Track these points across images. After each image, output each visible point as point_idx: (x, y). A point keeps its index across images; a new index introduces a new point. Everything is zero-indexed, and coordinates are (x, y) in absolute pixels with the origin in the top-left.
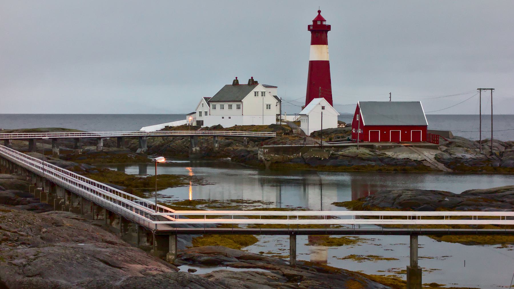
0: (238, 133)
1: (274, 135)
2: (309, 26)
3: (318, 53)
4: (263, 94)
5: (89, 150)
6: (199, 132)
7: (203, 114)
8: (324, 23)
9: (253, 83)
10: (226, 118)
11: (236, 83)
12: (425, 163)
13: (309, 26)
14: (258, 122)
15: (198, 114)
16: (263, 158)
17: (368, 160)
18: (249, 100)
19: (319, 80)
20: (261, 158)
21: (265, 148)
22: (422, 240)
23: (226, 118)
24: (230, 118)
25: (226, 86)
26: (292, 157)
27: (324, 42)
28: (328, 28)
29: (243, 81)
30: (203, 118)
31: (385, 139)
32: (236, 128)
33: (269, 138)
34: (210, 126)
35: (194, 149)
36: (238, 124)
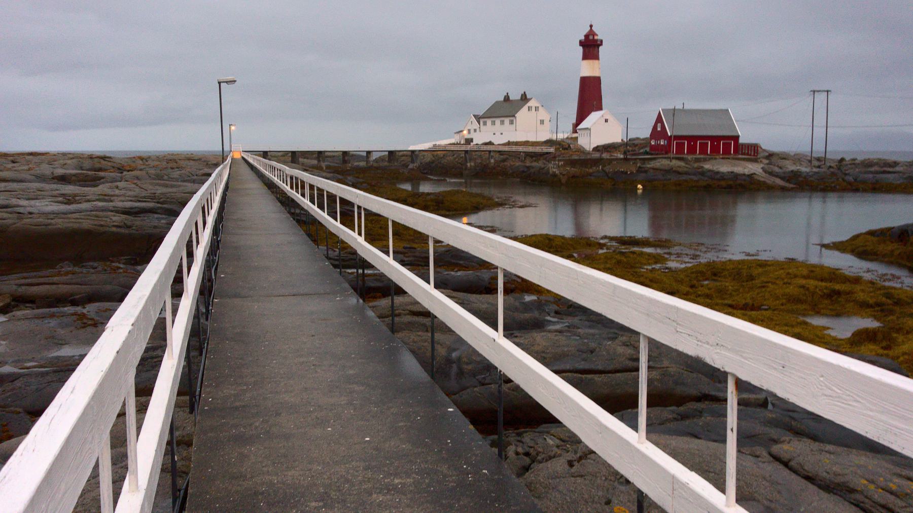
0: (514, 148)
1: (552, 150)
3: (588, 69)
4: (537, 109)
5: (358, 166)
6: (468, 148)
7: (472, 131)
8: (596, 38)
9: (524, 99)
10: (498, 134)
11: (507, 98)
12: (756, 177)
14: (532, 138)
15: (465, 132)
16: (557, 172)
17: (686, 173)
18: (523, 115)
19: (590, 96)
20: (554, 172)
21: (559, 161)
23: (498, 134)
25: (497, 102)
26: (591, 171)
27: (596, 57)
28: (601, 43)
29: (515, 96)
30: (473, 135)
31: (692, 150)
32: (509, 143)
33: (547, 153)
34: (480, 143)
35: (469, 165)
36: (511, 140)
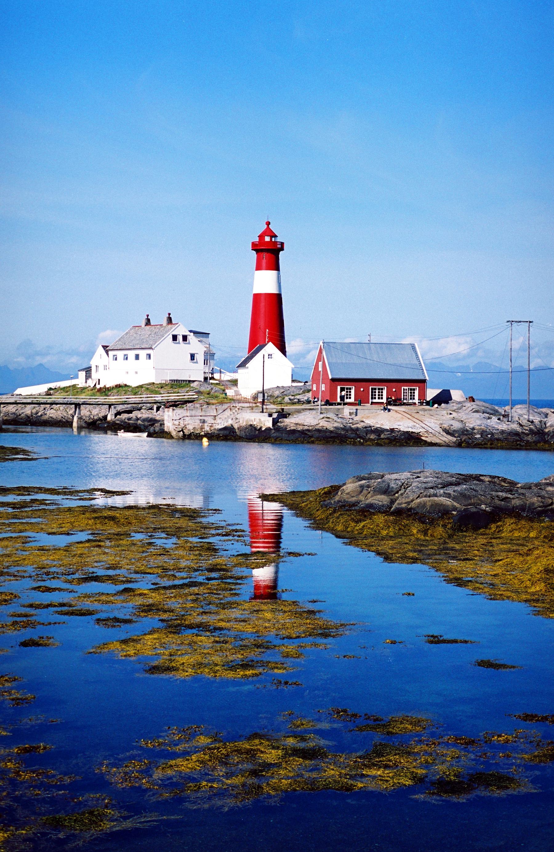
2: (253, 244)
3: (265, 282)
13: (253, 244)
19: (269, 321)
22: (262, 394)
24: (136, 373)
30: (428, 570)
